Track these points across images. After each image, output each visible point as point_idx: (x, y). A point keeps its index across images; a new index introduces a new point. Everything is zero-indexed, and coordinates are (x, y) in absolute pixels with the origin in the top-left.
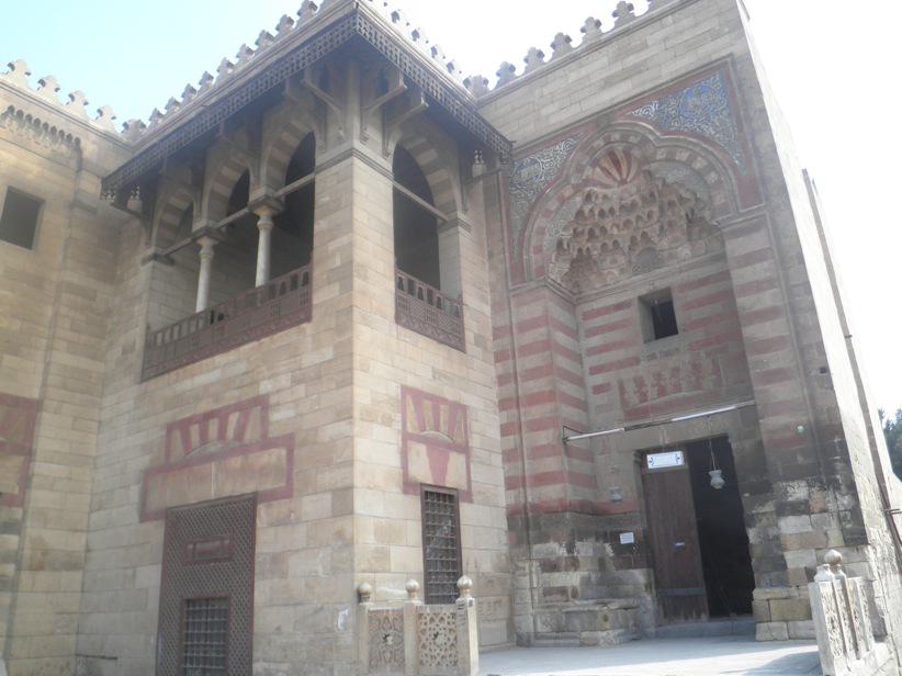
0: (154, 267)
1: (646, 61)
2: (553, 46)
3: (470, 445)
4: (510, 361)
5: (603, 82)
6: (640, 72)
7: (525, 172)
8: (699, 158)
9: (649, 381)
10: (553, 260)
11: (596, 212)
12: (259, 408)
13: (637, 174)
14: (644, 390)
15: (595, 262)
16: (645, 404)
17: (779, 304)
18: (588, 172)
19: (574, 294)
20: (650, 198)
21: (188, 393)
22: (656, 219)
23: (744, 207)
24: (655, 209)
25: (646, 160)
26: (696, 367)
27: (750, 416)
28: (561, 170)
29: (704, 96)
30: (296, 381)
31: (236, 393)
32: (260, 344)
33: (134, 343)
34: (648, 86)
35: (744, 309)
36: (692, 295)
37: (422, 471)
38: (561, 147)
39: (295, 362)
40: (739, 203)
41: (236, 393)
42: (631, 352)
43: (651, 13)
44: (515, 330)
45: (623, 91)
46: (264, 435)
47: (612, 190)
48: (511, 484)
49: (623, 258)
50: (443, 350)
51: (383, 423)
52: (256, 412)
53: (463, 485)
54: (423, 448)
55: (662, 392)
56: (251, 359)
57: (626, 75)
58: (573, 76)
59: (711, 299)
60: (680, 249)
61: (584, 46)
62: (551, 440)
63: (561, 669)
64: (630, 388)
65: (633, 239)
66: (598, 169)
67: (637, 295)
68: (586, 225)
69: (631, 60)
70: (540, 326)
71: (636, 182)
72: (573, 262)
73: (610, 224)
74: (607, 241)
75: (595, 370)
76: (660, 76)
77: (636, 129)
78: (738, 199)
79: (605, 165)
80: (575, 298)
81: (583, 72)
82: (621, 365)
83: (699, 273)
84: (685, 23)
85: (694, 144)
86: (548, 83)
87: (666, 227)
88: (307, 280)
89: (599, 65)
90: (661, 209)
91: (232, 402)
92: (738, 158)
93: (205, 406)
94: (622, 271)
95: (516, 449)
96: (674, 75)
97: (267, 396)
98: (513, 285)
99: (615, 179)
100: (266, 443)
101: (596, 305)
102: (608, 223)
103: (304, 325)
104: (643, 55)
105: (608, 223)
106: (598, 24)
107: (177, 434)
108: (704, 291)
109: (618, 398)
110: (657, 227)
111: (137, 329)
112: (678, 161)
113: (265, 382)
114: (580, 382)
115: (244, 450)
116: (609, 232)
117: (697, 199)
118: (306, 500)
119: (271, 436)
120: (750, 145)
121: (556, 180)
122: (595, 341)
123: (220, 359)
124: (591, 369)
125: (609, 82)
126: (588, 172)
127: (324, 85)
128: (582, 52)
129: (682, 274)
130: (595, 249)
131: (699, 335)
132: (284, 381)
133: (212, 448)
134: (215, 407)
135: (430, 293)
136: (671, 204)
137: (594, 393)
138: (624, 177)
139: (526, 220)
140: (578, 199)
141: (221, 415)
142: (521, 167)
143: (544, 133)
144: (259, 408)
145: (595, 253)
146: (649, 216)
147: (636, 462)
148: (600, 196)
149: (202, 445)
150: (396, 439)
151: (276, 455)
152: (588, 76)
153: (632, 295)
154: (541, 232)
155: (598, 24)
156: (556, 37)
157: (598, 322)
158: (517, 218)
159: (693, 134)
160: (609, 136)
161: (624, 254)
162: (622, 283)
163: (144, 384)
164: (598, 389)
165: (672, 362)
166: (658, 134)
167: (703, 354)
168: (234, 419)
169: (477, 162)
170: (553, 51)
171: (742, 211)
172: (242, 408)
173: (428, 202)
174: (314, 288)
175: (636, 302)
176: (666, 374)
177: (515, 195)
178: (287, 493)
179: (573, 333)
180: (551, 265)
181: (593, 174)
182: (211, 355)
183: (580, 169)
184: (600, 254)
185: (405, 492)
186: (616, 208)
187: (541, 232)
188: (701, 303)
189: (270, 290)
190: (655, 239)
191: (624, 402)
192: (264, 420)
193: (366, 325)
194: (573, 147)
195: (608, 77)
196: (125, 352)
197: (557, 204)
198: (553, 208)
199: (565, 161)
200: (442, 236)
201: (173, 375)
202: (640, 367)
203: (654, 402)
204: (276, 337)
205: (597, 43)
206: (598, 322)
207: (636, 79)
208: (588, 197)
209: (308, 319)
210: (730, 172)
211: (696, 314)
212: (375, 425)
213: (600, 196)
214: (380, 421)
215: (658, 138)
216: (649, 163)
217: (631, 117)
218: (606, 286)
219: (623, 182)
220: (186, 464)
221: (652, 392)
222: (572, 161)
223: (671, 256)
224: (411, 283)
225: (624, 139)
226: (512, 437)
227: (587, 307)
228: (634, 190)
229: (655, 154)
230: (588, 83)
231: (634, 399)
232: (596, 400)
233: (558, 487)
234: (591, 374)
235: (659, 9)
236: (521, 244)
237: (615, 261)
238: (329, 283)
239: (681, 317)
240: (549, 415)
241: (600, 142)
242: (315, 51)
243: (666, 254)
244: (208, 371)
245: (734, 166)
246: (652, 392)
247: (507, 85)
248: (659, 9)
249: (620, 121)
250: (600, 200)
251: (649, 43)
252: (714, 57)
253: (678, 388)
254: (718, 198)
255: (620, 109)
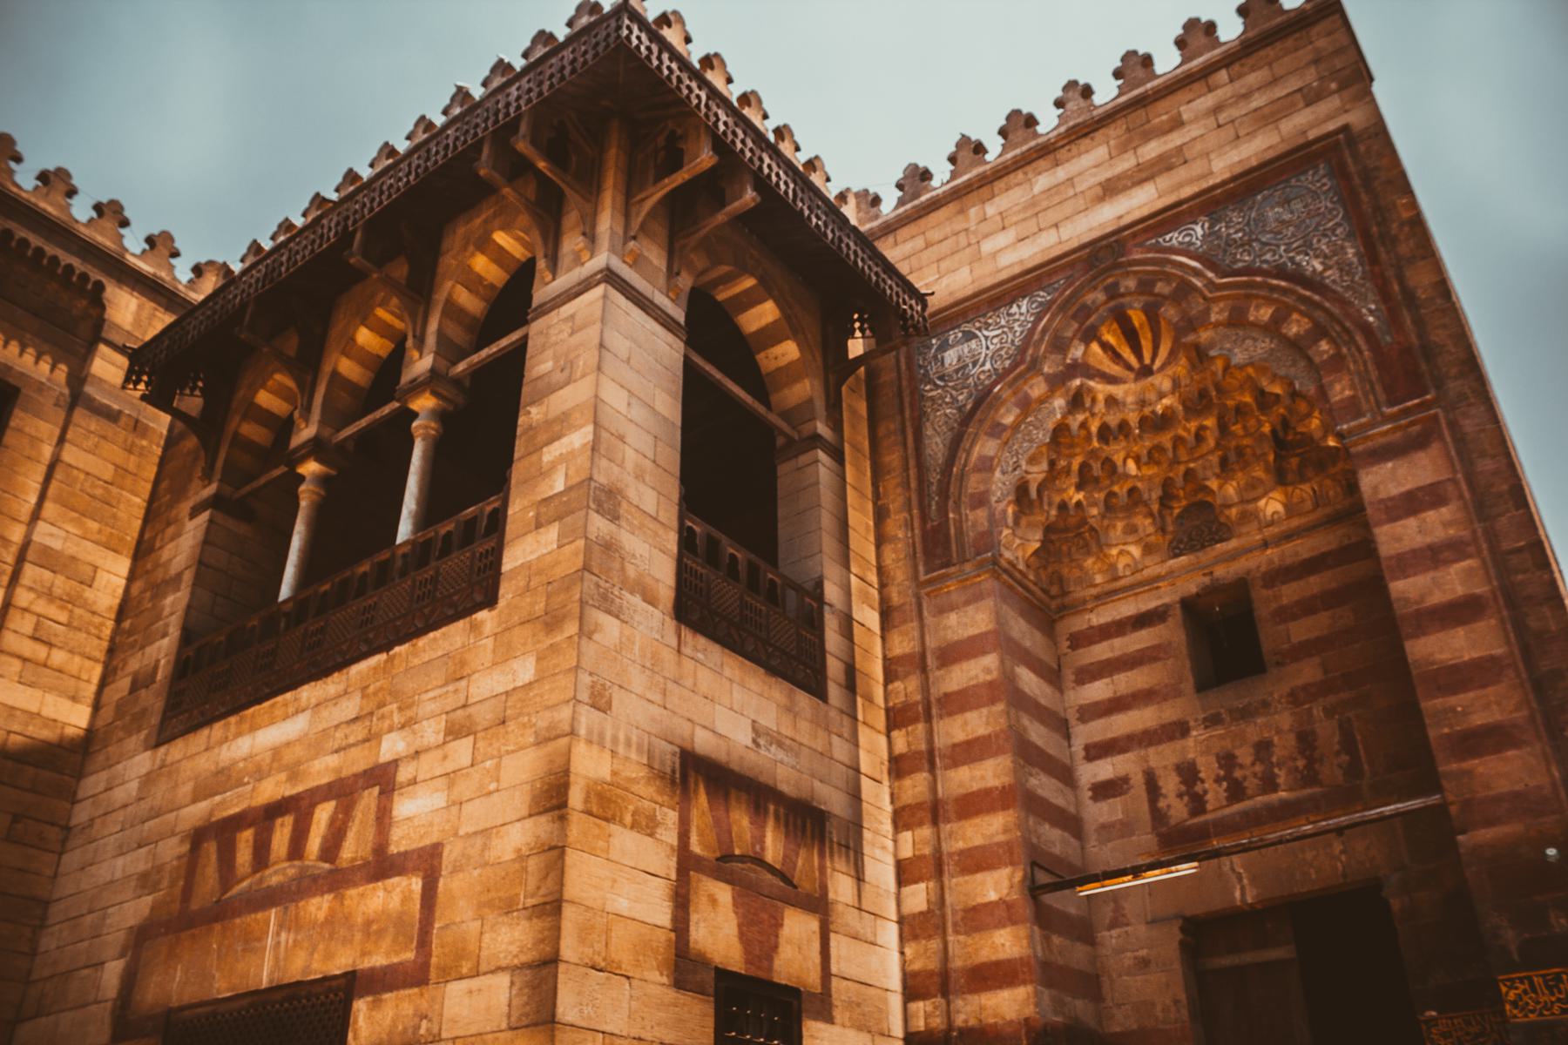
0: (211, 521)
1: (1180, 149)
2: (1003, 132)
3: (831, 895)
4: (920, 727)
5: (1099, 190)
6: (1170, 168)
7: (951, 357)
8: (1295, 316)
9: (1208, 768)
10: (1010, 521)
11: (1094, 428)
12: (376, 790)
13: (1173, 354)
14: (1198, 788)
15: (1092, 529)
16: (1202, 819)
17: (1481, 589)
18: (1077, 352)
19: (1053, 598)
20: (1198, 403)
21: (241, 765)
22: (1212, 443)
23: (1391, 404)
24: (1210, 422)
25: (1191, 324)
26: (1306, 740)
27: (1433, 832)
28: (1022, 350)
29: (1297, 206)
30: (454, 732)
31: (333, 761)
32: (390, 660)
33: (156, 667)
34: (1187, 192)
35: (1407, 600)
36: (1290, 593)
37: (718, 931)
38: (1023, 309)
39: (456, 691)
40: (1382, 397)
41: (333, 761)
42: (1169, 712)
43: (1186, 67)
44: (931, 661)
45: (1140, 201)
46: (380, 849)
47: (1126, 386)
48: (913, 989)
49: (1148, 521)
50: (778, 691)
51: (634, 826)
52: (369, 799)
53: (813, 979)
54: (725, 893)
55: (1236, 792)
56: (371, 689)
57: (1144, 175)
58: (1042, 182)
59: (1328, 600)
60: (1262, 503)
61: (1062, 129)
62: (1005, 891)
63: (425, 457)
64: (1170, 784)
65: (1167, 484)
66: (1095, 347)
67: (1176, 597)
68: (1073, 455)
69: (1152, 150)
70: (984, 653)
71: (1170, 371)
72: (1049, 529)
73: (1122, 454)
74: (1116, 488)
75: (1096, 751)
76: (1211, 173)
77: (1168, 269)
78: (1378, 388)
79: (1110, 338)
80: (1054, 604)
81: (1061, 173)
82: (1146, 738)
83: (1304, 548)
84: (1252, 79)
85: (1284, 291)
86: (993, 196)
87: (1232, 457)
88: (497, 522)
89: (1092, 162)
90: (1223, 427)
91: (325, 780)
92: (1371, 311)
93: (272, 789)
94: (1148, 550)
95: (929, 911)
96: (1238, 170)
97: (395, 763)
98: (927, 573)
99: (1129, 367)
100: (383, 866)
101: (1100, 617)
102: (1117, 451)
103: (483, 615)
104: (1176, 139)
105: (1117, 451)
106: (1087, 92)
107: (211, 849)
108: (1314, 584)
109: (1146, 807)
110: (1214, 459)
111: (166, 641)
112: (1253, 325)
113: (393, 735)
114: (1066, 775)
115: (337, 881)
116: (1120, 470)
117: (1295, 395)
118: (455, 989)
119: (393, 849)
120: (1396, 287)
121: (1014, 366)
122: (1098, 690)
123: (308, 693)
124: (1087, 748)
125: (1110, 189)
126: (1077, 352)
127: (557, 156)
128: (1060, 137)
129: (1269, 552)
130: (1095, 504)
131: (1308, 672)
132: (431, 731)
133: (275, 877)
134: (289, 791)
135: (753, 569)
136: (1240, 410)
137: (1095, 798)
138: (1133, 360)
139: (955, 445)
140: (1059, 403)
141: (297, 807)
142: (945, 346)
143: (989, 282)
144: (376, 790)
145: (1094, 511)
146: (1199, 437)
147: (1181, 943)
148: (1101, 397)
149: (255, 871)
150: (669, 866)
151: (393, 896)
152: (1070, 179)
153: (1166, 596)
154: (987, 465)
155: (1087, 92)
156: (1008, 118)
157: (1101, 651)
158: (936, 445)
159: (1280, 272)
160: (1116, 285)
161: (1151, 514)
162: (1146, 573)
163: (162, 749)
164: (1103, 790)
165: (1253, 731)
166: (1210, 275)
167: (1317, 712)
168: (323, 814)
169: (858, 334)
170: (1001, 140)
171: (1388, 411)
172: (343, 791)
173: (759, 400)
174: (509, 535)
175: (1178, 611)
176: (1245, 755)
177: (932, 399)
178: (416, 976)
179: (1053, 676)
180: (1006, 532)
181: (1085, 353)
182: (294, 685)
183: (1060, 346)
184: (1103, 517)
185: (680, 982)
186: (1133, 418)
187: (987, 465)
188: (1306, 608)
189: (421, 551)
190: (1213, 484)
191: (1158, 816)
192: (383, 817)
193: (609, 612)
194: (1046, 307)
195: (1109, 180)
196: (135, 687)
197: (1017, 411)
198: (1008, 420)
199: (1032, 331)
200: (783, 469)
201: (218, 729)
202: (1190, 742)
203: (1219, 814)
204: (422, 642)
205: (1085, 122)
206: (1101, 651)
207: (1164, 181)
208: (1077, 401)
209: (490, 601)
210: (1360, 339)
211: (1301, 630)
212: (614, 828)
213: (1101, 397)
214: (628, 819)
215: (1210, 282)
216: (1194, 330)
217: (1158, 248)
218: (1117, 578)
219: (1146, 371)
220: (222, 912)
221: (1214, 794)
222: (1044, 331)
223: (1245, 517)
224: (712, 544)
225: (1145, 286)
226: (922, 886)
227: (1078, 623)
228: (1166, 385)
229: (1207, 311)
230: (1071, 192)
231: (1177, 809)
232: (1099, 813)
233: (1022, 992)
234: (1095, 798)
235: (1201, 59)
236: (944, 493)
237: (1131, 530)
238: (538, 526)
239: (1270, 637)
240: (1001, 838)
241: (1100, 296)
242: (540, 84)
243: (1234, 512)
244: (286, 717)
245: (1366, 329)
246: (1214, 794)
247: (916, 202)
248: (1201, 59)
249: (1137, 256)
250: (1100, 406)
251: (1185, 117)
252: (1312, 135)
253: (1269, 784)
254: (1338, 387)
255: (1134, 235)
